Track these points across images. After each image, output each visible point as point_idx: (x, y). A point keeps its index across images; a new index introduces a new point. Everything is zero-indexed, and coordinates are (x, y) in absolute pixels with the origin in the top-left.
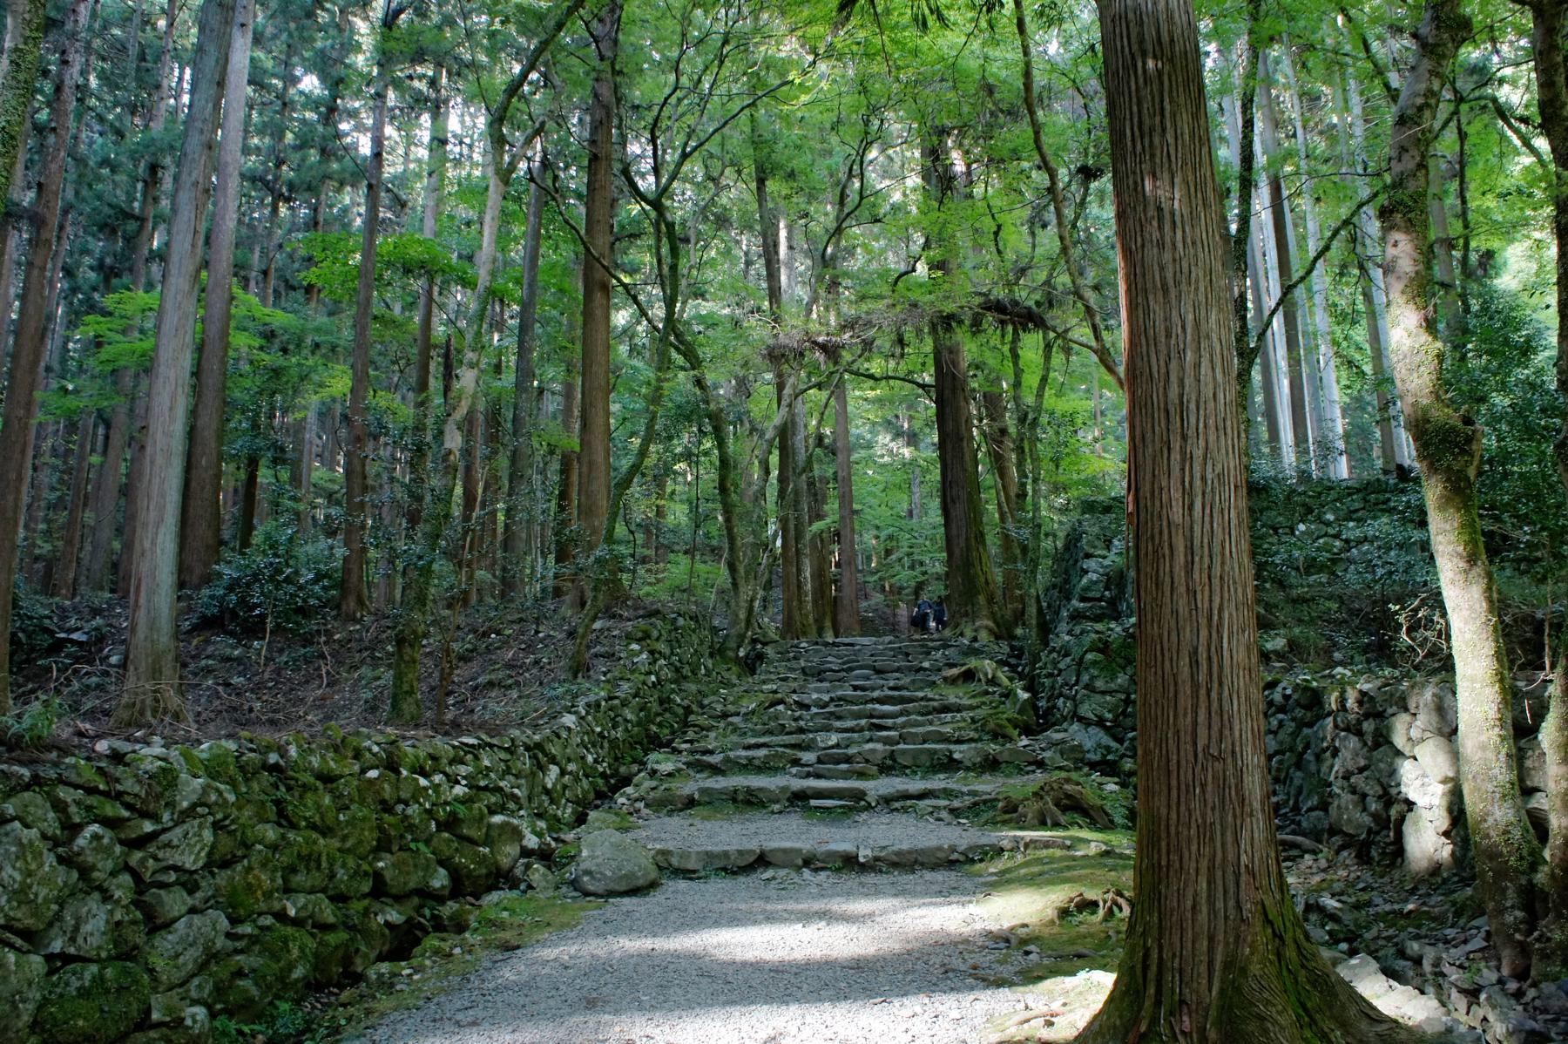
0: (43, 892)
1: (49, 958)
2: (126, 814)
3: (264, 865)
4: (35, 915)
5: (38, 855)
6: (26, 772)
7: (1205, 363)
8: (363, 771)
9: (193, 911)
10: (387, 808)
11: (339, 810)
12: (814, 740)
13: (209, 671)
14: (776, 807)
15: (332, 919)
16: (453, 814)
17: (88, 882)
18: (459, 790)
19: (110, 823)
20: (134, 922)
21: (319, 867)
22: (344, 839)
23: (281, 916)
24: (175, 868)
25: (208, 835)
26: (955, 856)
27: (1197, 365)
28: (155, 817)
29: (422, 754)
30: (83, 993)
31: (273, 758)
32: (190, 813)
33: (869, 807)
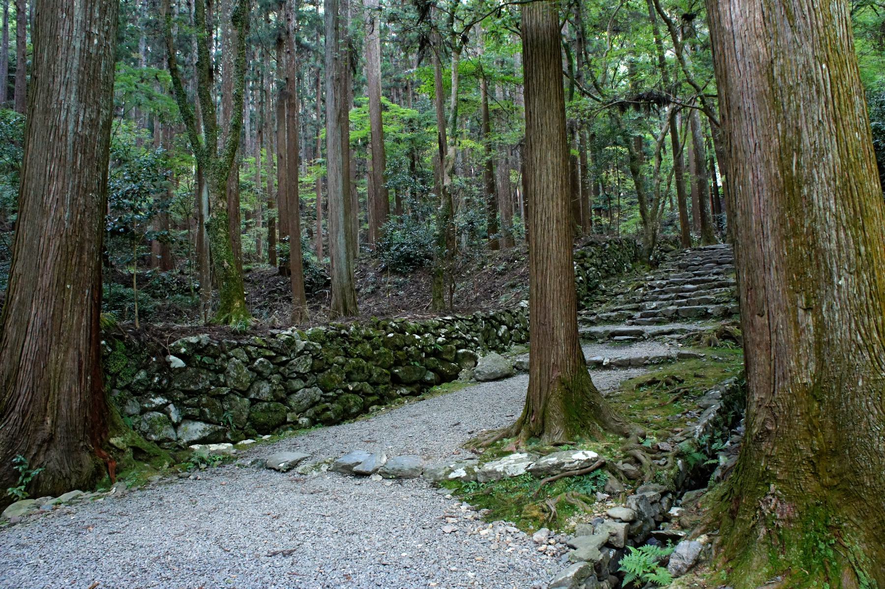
0: (244, 379)
1: (251, 399)
2: (274, 354)
3: (337, 372)
4: (242, 385)
5: (241, 368)
6: (235, 342)
7: (544, 173)
8: (387, 334)
9: (306, 387)
10: (400, 348)
11: (373, 350)
12: (644, 306)
13: (389, 290)
14: (600, 340)
15: (371, 392)
16: (436, 349)
17: (260, 376)
18: (440, 339)
19: (269, 358)
20: (280, 390)
21: (363, 372)
22: (377, 361)
23: (346, 390)
24: (296, 372)
25: (309, 361)
26: (647, 361)
27: (540, 176)
28: (285, 355)
29: (418, 326)
30: (262, 411)
31: (343, 332)
32: (301, 353)
33: (644, 339)
